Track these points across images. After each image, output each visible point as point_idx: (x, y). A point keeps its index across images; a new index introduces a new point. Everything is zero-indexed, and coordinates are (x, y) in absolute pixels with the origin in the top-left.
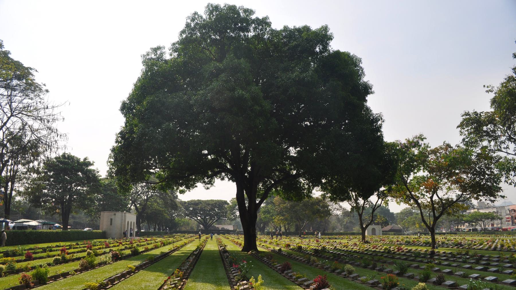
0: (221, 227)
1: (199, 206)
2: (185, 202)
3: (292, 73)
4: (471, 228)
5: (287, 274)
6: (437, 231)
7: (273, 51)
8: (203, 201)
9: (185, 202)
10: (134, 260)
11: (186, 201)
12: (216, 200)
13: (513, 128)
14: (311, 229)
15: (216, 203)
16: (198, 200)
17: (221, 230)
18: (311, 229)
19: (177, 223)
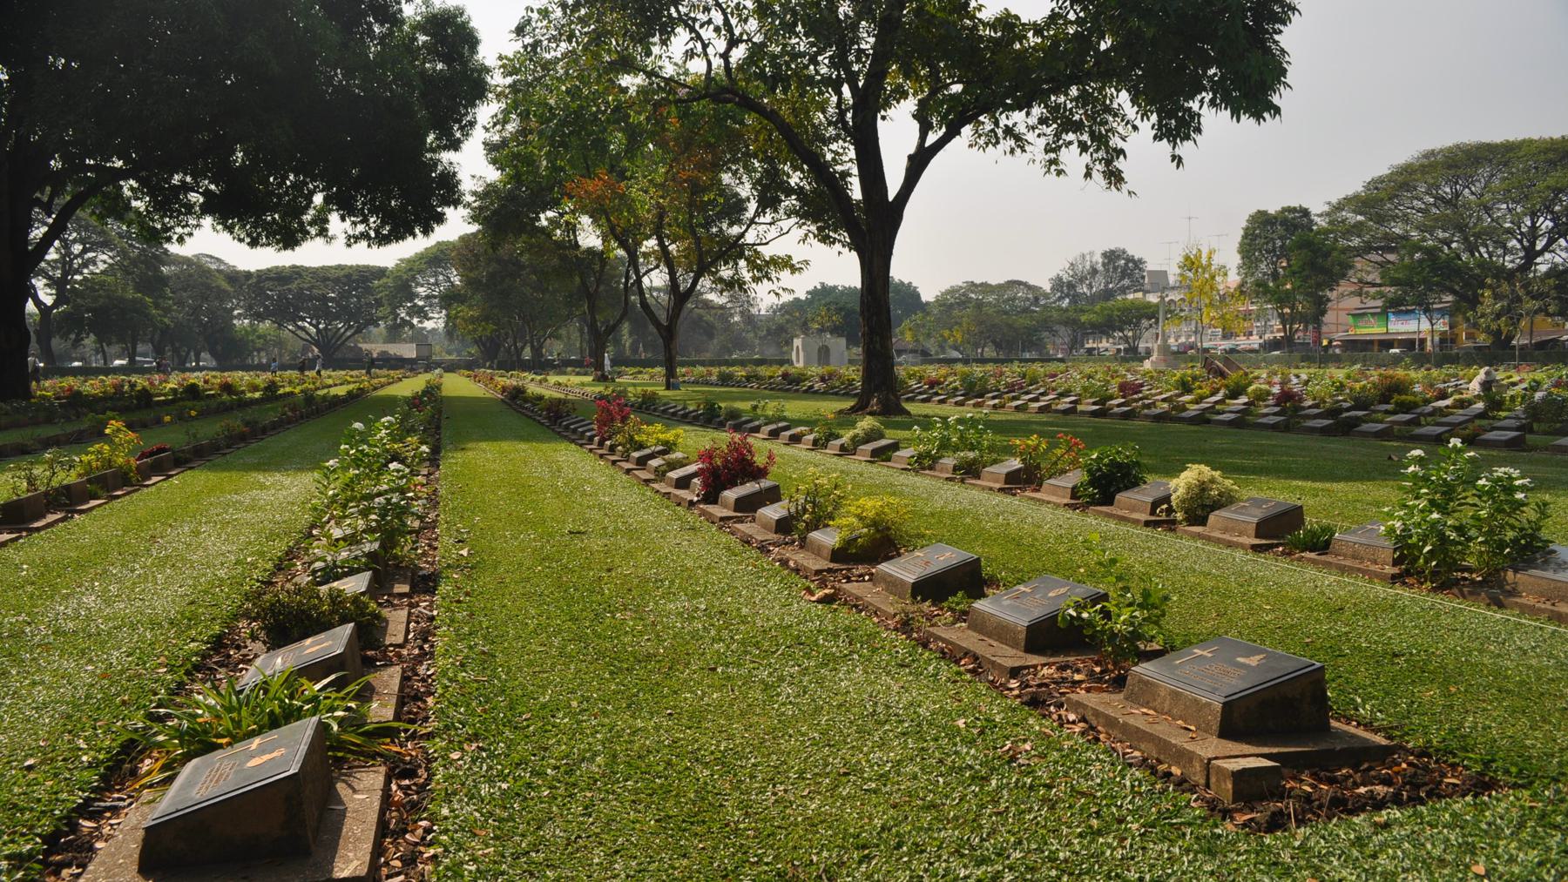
0: (378, 350)
1: (294, 286)
2: (249, 272)
3: (731, 225)
4: (1122, 347)
5: (645, 464)
6: (679, 358)
7: (572, 101)
8: (307, 269)
9: (248, 275)
10: (265, 466)
11: (253, 270)
12: (351, 267)
13: (956, 449)
14: (641, 349)
15: (348, 276)
16: (294, 267)
17: (378, 359)
18: (641, 349)
19: (240, 340)
